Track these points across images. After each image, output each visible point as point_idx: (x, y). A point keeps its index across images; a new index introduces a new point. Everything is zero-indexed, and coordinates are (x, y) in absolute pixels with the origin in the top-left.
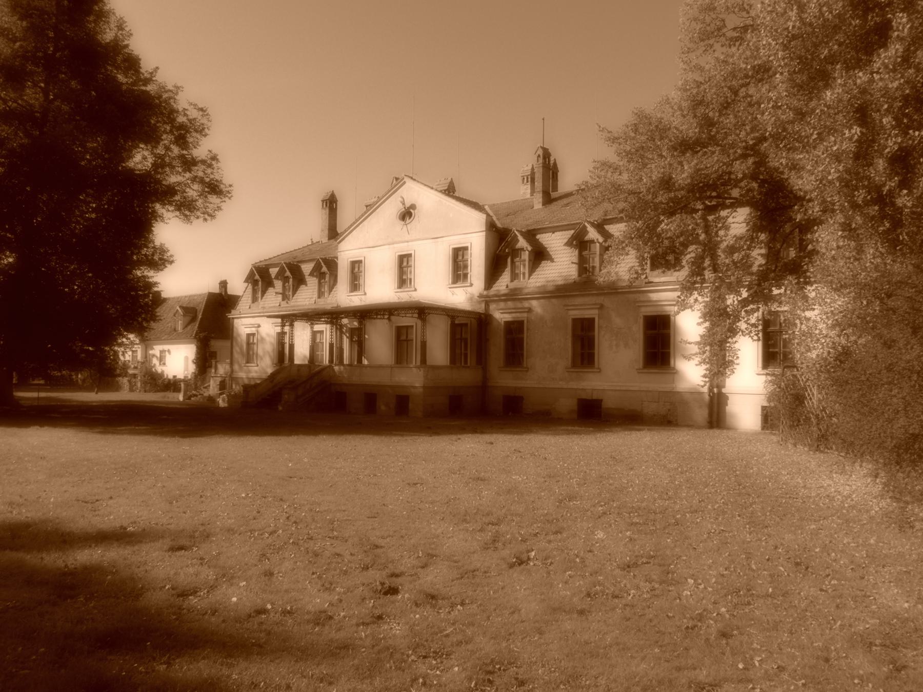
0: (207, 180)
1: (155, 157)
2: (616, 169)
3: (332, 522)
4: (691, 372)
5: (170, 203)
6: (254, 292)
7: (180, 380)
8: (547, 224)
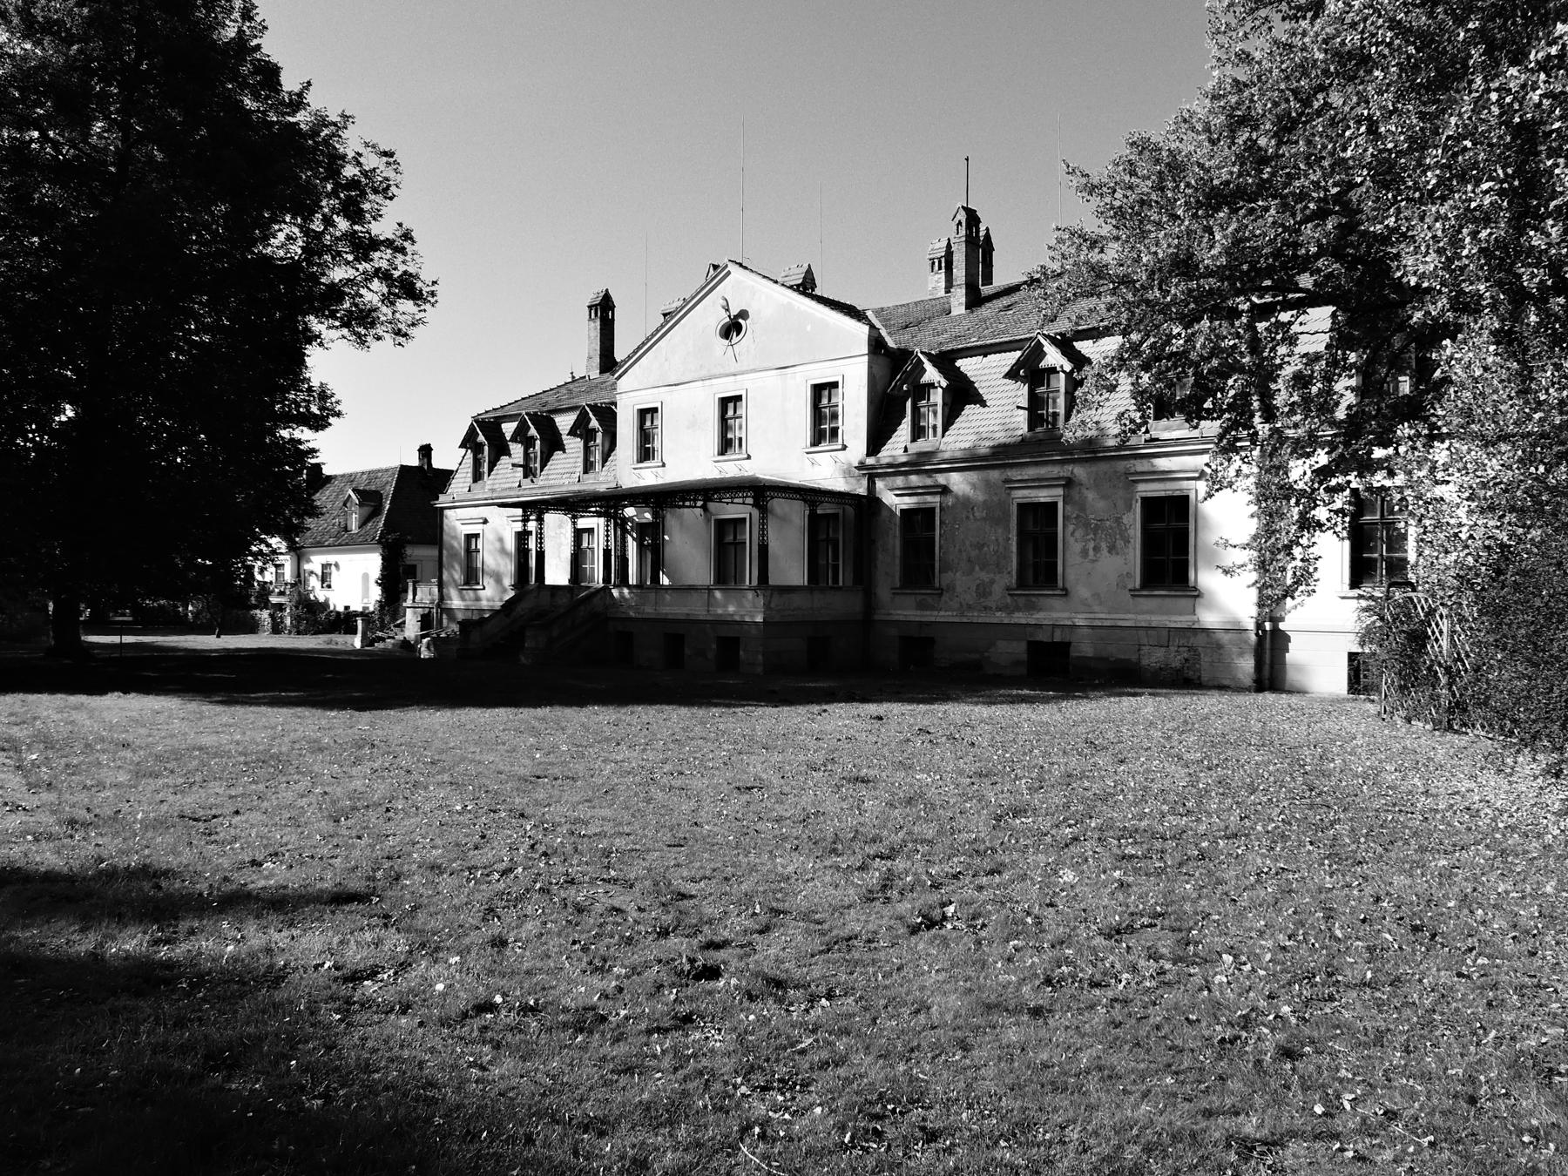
0: (396, 274)
2: (1095, 243)
3: (607, 853)
5: (333, 315)
6: (477, 464)
7: (357, 614)
8: (974, 342)
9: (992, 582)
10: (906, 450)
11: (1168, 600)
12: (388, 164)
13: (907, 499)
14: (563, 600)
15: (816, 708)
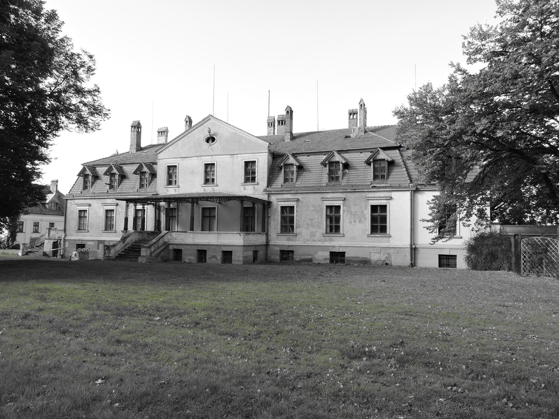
6: (85, 182)
8: (304, 151)
9: (316, 232)
10: (282, 186)
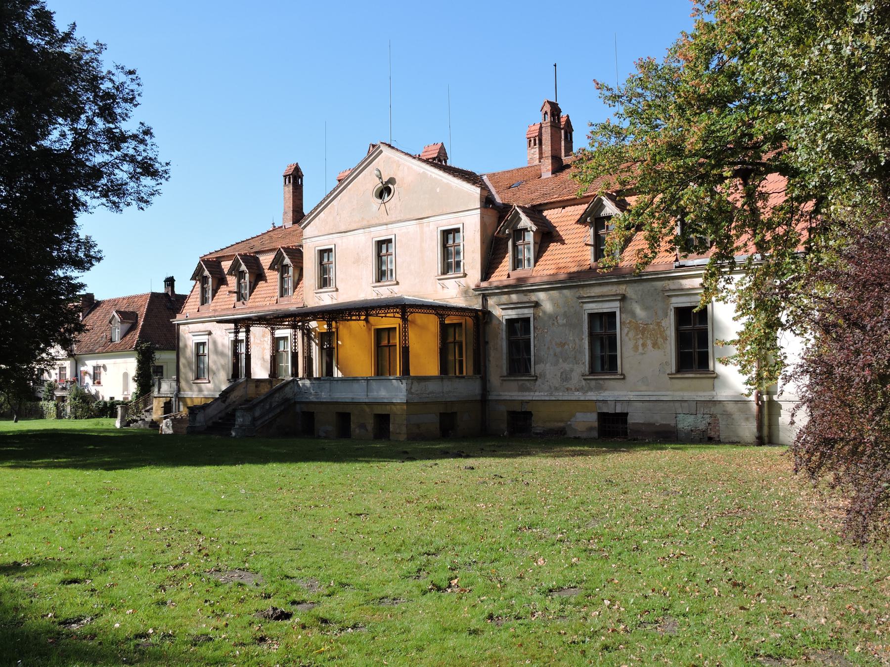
0: (140, 158)
1: (76, 133)
2: (618, 133)
3: (248, 554)
4: (733, 379)
5: (95, 188)
6: (204, 291)
7: (118, 403)
8: (555, 198)
9: (572, 370)
10: (509, 276)
11: (695, 381)
12: (132, 80)
13: (510, 312)
14: (265, 390)
15: (429, 462)
